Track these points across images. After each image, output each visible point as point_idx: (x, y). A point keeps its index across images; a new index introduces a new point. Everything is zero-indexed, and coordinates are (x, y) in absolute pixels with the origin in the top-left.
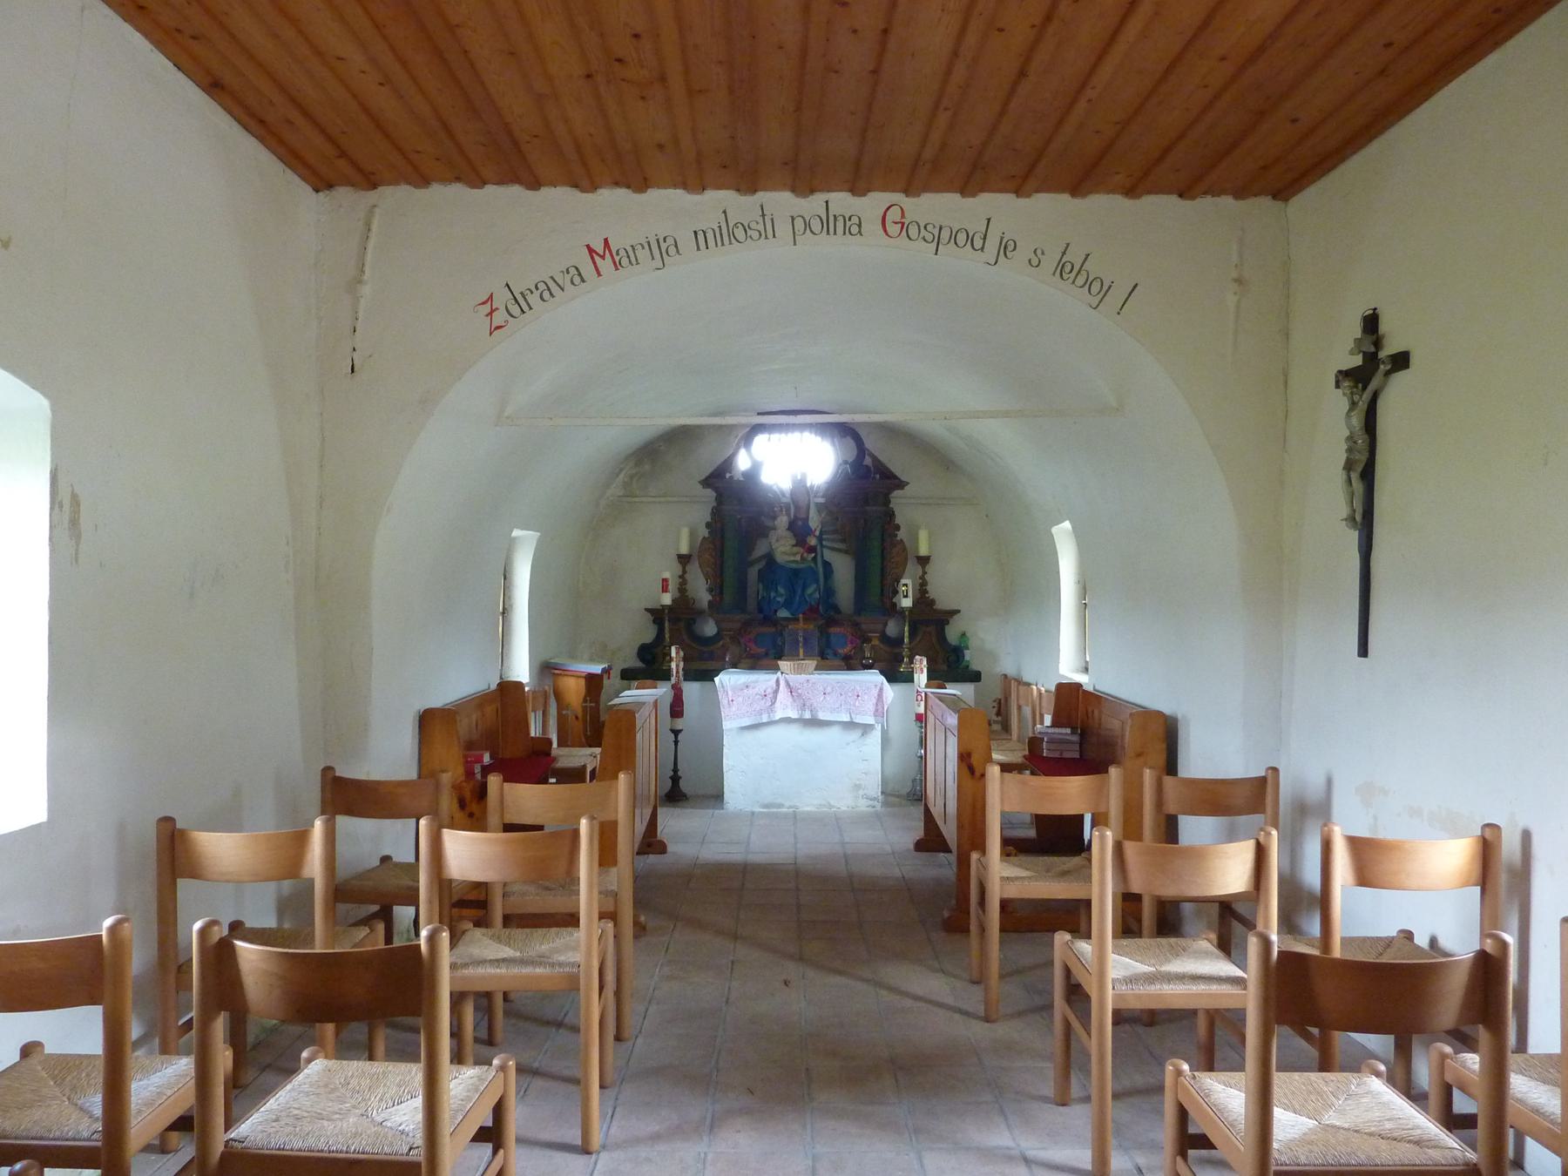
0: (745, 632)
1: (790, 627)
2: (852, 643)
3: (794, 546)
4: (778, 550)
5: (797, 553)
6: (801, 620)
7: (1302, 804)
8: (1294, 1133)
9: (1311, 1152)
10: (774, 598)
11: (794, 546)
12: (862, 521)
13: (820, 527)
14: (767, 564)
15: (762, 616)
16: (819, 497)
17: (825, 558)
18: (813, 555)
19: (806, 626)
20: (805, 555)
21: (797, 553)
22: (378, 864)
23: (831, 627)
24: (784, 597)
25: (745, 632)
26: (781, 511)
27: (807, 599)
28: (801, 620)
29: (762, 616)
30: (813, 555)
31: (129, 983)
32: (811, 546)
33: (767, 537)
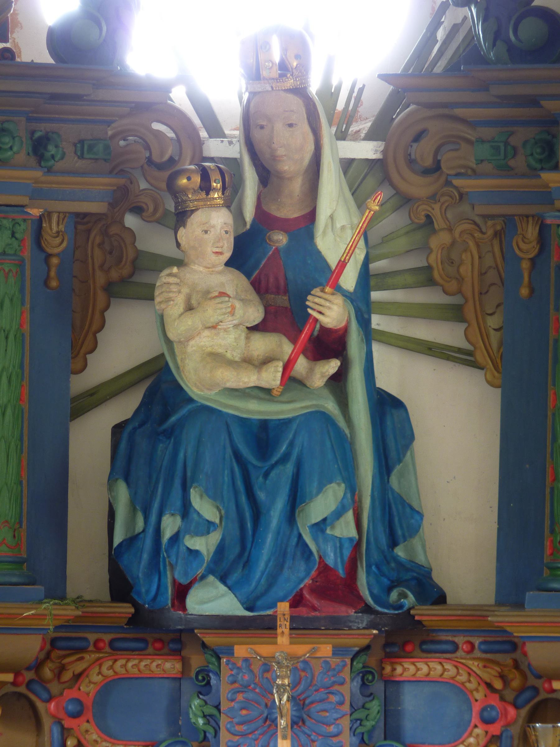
0: (58, 675)
1: (241, 651)
2: (487, 722)
3: (253, 329)
4: (193, 346)
5: (266, 361)
6: (284, 626)
7: (163, 353)
8: (223, 325)
9: (255, 361)
10: (176, 538)
11: (253, 329)
12: (532, 232)
13: (360, 255)
14: (146, 403)
15: (127, 609)
16: (356, 137)
17: (382, 383)
18: (333, 365)
19: (302, 650)
20: (302, 364)
21: (266, 361)
22: (378, 386)
23: (408, 656)
24: (215, 538)
25: (58, 675)
26: (206, 188)
27: (308, 539)
28: (284, 626)
29: (127, 609)
30: (333, 365)
31: (113, 549)
32: (324, 330)
33: (151, 298)
